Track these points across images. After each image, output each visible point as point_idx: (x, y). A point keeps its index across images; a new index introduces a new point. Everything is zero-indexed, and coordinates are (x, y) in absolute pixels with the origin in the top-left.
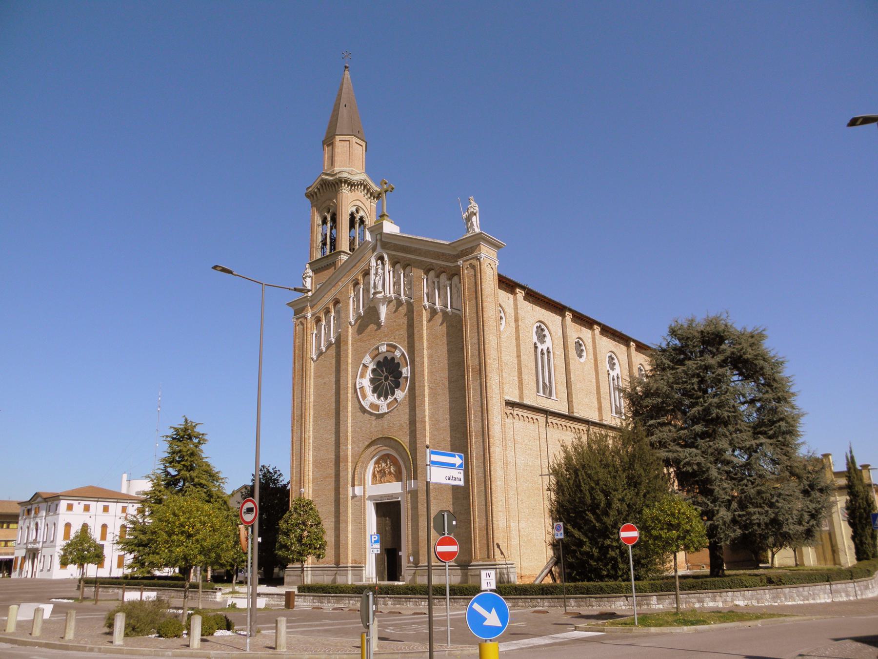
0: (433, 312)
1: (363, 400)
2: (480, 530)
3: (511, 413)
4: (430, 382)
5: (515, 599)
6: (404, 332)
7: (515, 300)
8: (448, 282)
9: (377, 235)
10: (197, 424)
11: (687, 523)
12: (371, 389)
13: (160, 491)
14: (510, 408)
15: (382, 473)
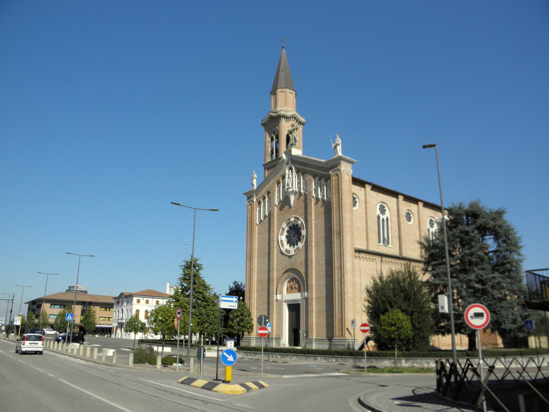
0: (317, 200)
1: (282, 247)
2: (338, 320)
3: (358, 256)
4: (315, 239)
5: (337, 357)
6: (302, 211)
7: (365, 191)
8: (325, 183)
9: (289, 155)
10: (197, 259)
11: (400, 324)
12: (286, 242)
13: (178, 295)
14: (358, 253)
15: (291, 288)
